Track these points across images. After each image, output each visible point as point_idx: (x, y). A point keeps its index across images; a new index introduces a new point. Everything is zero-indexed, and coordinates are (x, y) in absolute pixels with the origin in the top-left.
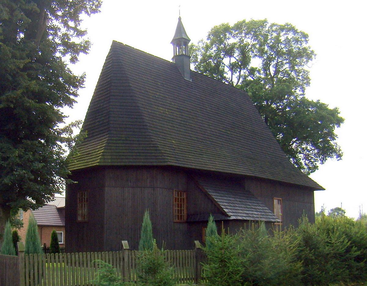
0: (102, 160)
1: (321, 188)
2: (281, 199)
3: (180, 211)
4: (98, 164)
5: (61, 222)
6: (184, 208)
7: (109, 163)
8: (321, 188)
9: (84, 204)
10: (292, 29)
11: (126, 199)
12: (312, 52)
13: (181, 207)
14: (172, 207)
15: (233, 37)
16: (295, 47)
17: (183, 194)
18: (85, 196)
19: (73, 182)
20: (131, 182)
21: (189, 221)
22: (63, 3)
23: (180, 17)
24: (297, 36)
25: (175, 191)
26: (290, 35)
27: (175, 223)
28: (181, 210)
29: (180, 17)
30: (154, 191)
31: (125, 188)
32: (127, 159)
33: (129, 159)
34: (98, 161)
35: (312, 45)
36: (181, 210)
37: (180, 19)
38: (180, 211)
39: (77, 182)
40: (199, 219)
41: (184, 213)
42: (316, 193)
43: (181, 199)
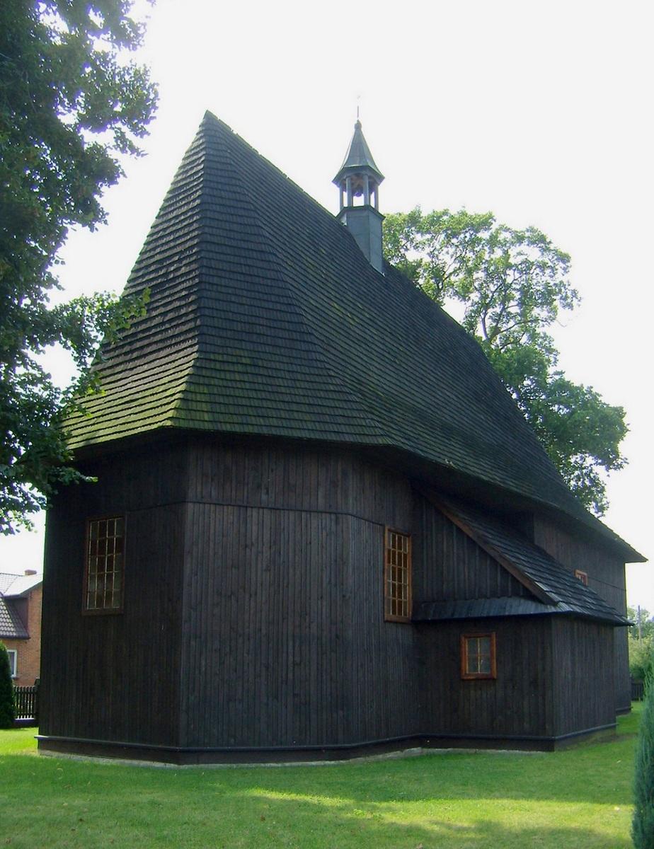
0: (183, 412)
1: (639, 558)
2: (585, 574)
3: (398, 590)
4: (169, 423)
5: (12, 630)
6: (407, 580)
7: (204, 421)
8: (639, 558)
9: (110, 560)
10: (540, 240)
11: (252, 544)
12: (574, 293)
13: (400, 580)
14: (380, 575)
15: (416, 247)
16: (539, 280)
17: (405, 540)
18: (111, 533)
19: (84, 477)
20: (267, 493)
21: (419, 618)
22: (1, 346)
23: (358, 121)
24: (547, 258)
25: (389, 530)
26: (534, 254)
27: (387, 625)
28: (400, 586)
29: (358, 121)
30: (337, 523)
31: (249, 510)
32: (263, 417)
33: (268, 417)
34: (170, 414)
35: (575, 278)
36: (400, 586)
37: (358, 126)
38: (398, 590)
39: (94, 479)
40: (453, 615)
41: (405, 598)
42: (629, 567)
43: (400, 554)
